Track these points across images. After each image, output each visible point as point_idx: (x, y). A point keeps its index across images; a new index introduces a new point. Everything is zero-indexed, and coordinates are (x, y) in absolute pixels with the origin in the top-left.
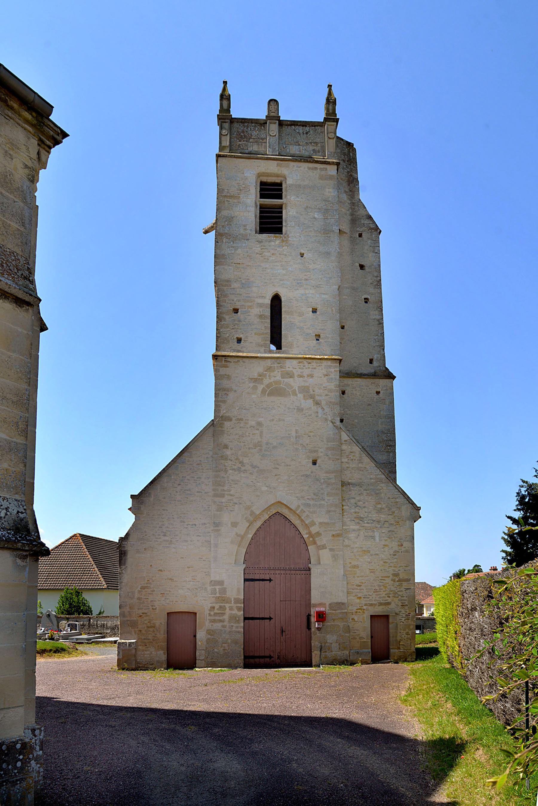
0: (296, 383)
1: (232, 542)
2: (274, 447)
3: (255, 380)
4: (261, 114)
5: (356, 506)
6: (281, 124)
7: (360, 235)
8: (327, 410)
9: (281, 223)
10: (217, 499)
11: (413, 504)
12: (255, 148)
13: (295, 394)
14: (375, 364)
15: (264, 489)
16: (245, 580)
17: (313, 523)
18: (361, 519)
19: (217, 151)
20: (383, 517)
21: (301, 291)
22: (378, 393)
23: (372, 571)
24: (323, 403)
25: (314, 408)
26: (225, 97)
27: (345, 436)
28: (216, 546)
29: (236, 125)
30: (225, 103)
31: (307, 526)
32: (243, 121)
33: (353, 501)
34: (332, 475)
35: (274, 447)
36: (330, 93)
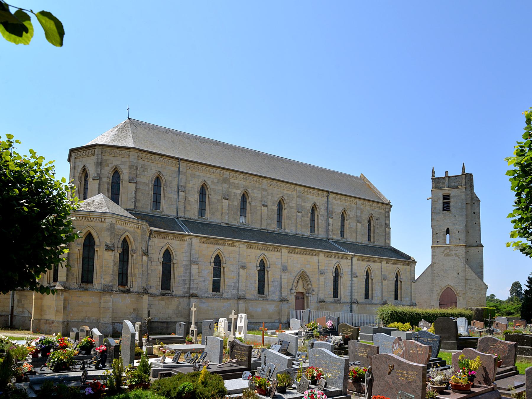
0: (453, 253)
1: (436, 295)
2: (447, 270)
3: (442, 252)
4: (444, 176)
5: (470, 285)
6: (449, 177)
7: (474, 203)
8: (462, 259)
9: (449, 207)
10: (433, 284)
11: (486, 285)
12: (442, 186)
13: (453, 255)
14: (478, 242)
15: (445, 281)
16: (440, 305)
17: (458, 290)
18: (471, 289)
19: (431, 189)
20: (477, 288)
21: (455, 227)
22: (478, 251)
23: (474, 303)
24: (461, 258)
25: (458, 259)
26: (433, 172)
27: (467, 266)
28: (432, 296)
29: (436, 179)
30: (433, 174)
31: (456, 291)
32: (438, 178)
33: (469, 284)
34: (463, 277)
35: (447, 270)
36: (463, 166)
